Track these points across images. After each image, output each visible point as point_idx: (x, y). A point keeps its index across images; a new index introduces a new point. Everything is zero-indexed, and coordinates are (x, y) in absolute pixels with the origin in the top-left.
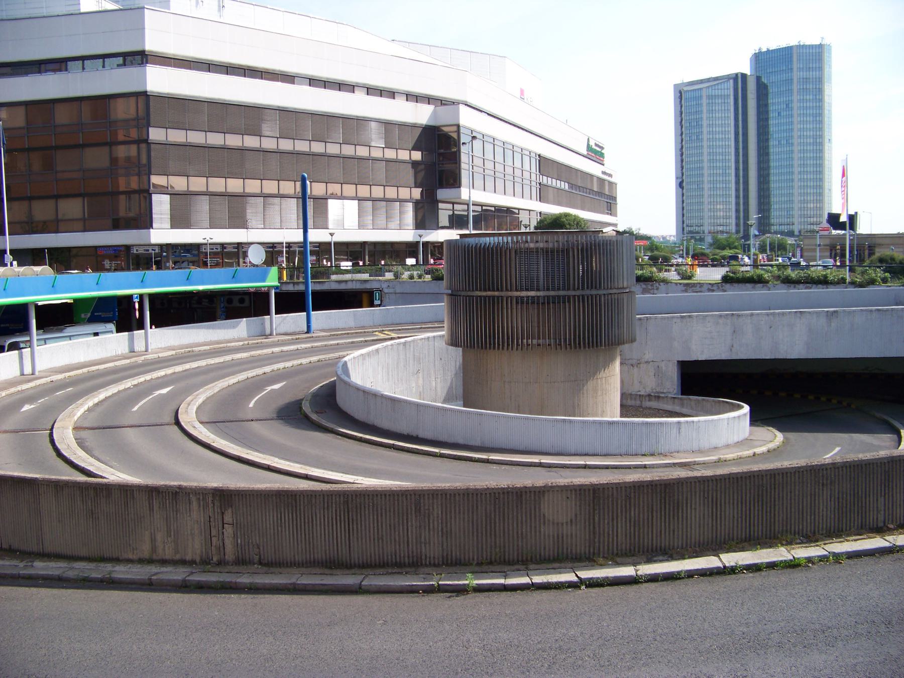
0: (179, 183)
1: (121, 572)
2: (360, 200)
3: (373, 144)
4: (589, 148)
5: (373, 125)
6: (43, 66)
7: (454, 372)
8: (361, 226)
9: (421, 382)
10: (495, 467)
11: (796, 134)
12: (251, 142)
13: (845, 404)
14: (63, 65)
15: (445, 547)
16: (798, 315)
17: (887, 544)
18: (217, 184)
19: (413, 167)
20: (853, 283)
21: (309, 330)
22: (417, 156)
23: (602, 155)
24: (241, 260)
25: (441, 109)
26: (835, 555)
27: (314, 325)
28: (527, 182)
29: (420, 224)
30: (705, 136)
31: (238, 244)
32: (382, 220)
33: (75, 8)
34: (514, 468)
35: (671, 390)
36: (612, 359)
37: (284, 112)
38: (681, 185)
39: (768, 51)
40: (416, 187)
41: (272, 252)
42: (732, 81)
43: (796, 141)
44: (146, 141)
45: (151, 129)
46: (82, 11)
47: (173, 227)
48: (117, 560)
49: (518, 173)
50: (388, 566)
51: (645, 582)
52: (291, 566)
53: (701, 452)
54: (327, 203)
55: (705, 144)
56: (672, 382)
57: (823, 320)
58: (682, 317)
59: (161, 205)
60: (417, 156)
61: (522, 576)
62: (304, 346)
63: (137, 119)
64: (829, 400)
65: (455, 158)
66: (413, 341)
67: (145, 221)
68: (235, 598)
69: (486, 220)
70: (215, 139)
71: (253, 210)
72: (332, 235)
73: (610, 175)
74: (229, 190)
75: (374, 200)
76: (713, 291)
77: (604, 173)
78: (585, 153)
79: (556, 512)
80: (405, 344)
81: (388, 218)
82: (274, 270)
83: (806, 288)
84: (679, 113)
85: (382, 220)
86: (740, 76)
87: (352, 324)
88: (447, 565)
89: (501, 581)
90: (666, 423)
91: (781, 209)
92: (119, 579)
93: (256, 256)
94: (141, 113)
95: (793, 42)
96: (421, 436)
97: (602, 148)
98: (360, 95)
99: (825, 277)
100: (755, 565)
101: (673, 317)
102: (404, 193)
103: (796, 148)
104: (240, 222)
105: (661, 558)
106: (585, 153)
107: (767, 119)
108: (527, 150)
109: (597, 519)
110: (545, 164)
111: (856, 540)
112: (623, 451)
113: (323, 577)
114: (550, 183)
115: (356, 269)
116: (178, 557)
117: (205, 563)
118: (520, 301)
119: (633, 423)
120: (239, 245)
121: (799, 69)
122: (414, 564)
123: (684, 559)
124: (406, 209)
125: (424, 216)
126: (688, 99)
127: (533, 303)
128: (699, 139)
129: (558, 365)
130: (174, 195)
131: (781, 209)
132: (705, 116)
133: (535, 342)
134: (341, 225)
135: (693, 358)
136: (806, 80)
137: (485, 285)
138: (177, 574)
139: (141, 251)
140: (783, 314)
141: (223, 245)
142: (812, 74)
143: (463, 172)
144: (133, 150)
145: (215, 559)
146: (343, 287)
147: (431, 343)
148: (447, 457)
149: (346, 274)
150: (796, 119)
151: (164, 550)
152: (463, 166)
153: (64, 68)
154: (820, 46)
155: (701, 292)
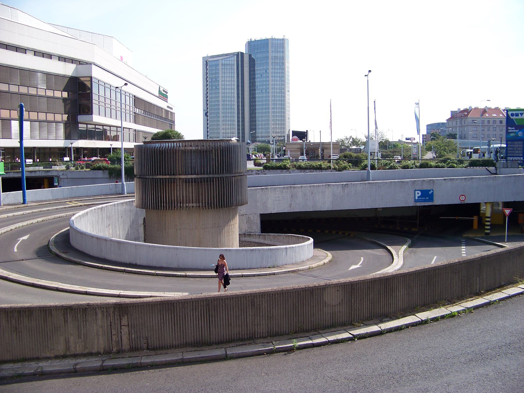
1: (47, 366)
3: (39, 87)
7: (129, 225)
9: (111, 231)
10: (192, 279)
11: (270, 87)
13: (347, 234)
15: (269, 326)
16: (327, 186)
17: (487, 301)
19: (63, 102)
20: (335, 169)
21: (24, 203)
22: (65, 95)
23: (167, 97)
26: (468, 308)
27: (27, 199)
28: (128, 112)
29: (68, 136)
30: (220, 87)
32: (45, 134)
34: (203, 279)
35: (257, 231)
38: (206, 114)
42: (235, 56)
43: (270, 91)
48: (38, 359)
50: (234, 341)
51: (386, 333)
52: (170, 348)
53: (297, 264)
54: (11, 123)
55: (220, 91)
56: (257, 227)
57: (340, 189)
60: (65, 95)
61: (320, 338)
62: (27, 212)
64: (337, 233)
65: (89, 97)
66: (106, 206)
68: (145, 373)
72: (111, 145)
73: (171, 108)
75: (40, 122)
76: (259, 174)
77: (168, 107)
78: (158, 95)
79: (332, 299)
80: (102, 208)
81: (49, 132)
83: (310, 172)
84: (205, 74)
85: (45, 134)
86: (240, 53)
87: (51, 198)
88: (270, 336)
89: (310, 342)
90: (280, 249)
91: (262, 129)
92: (50, 371)
95: (269, 37)
96: (138, 263)
97: (167, 93)
99: (321, 165)
100: (435, 318)
101: (257, 189)
102: (58, 117)
105: (386, 319)
106: (158, 95)
107: (254, 78)
109: (353, 301)
110: (137, 101)
111: (472, 300)
112: (258, 266)
113: (201, 352)
115: (35, 164)
116: (86, 351)
117: (108, 353)
118: (186, 181)
119: (264, 250)
122: (251, 338)
123: (399, 318)
124: (59, 127)
125: (70, 131)
126: (211, 66)
128: (217, 88)
129: (209, 218)
131: (262, 129)
132: (220, 75)
133: (191, 205)
136: (276, 57)
137: (171, 172)
138: (95, 363)
140: (319, 186)
142: (279, 55)
143: (94, 105)
145: (115, 350)
146: (33, 175)
147: (116, 208)
148: (179, 277)
149: (31, 167)
150: (270, 79)
151: (75, 347)
152: (94, 101)
154: (283, 40)
155: (252, 175)
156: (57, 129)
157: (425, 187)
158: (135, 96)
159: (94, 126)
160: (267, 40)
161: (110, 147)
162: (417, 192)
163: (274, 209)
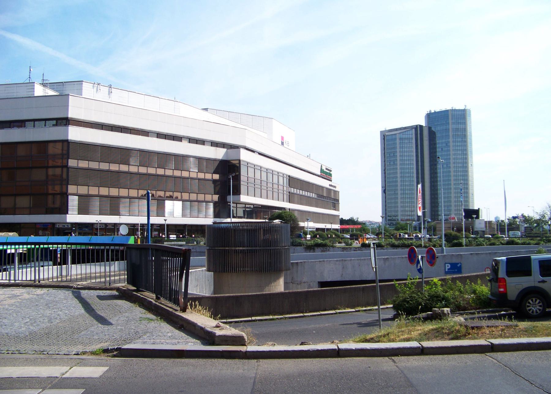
0: (83, 190)
2: (183, 201)
3: (191, 170)
4: (322, 170)
5: (192, 159)
6: (12, 124)
8: (184, 215)
12: (124, 168)
14: (23, 124)
18: (104, 191)
22: (216, 177)
23: (331, 175)
24: (116, 233)
25: (231, 151)
31: (115, 224)
32: (195, 213)
33: (32, 93)
36: (278, 278)
37: (142, 152)
38: (384, 191)
39: (435, 113)
40: (215, 194)
41: (133, 229)
42: (414, 130)
43: (452, 165)
44: (66, 166)
45: (69, 160)
46: (35, 95)
47: (79, 214)
49: (275, 186)
55: (398, 167)
58: (320, 261)
59: (73, 201)
60: (216, 177)
63: (62, 155)
65: (237, 179)
67: (64, 210)
69: (256, 213)
70: (104, 166)
71: (124, 206)
72: (165, 220)
73: (335, 187)
74: (111, 194)
77: (330, 185)
82: (132, 238)
85: (195, 213)
93: (124, 230)
94: (65, 152)
95: (449, 108)
97: (331, 171)
98: (185, 143)
102: (209, 197)
103: (452, 170)
104: (115, 212)
106: (319, 174)
108: (281, 173)
110: (292, 181)
114: (295, 192)
120: (115, 225)
121: (453, 123)
124: (209, 206)
125: (219, 211)
127: (241, 252)
128: (395, 164)
130: (80, 196)
132: (398, 150)
134: (172, 214)
135: (325, 280)
136: (457, 130)
139: (61, 226)
141: (106, 224)
142: (461, 126)
144: (58, 171)
152: (242, 183)
153: (23, 125)
154: (464, 110)
156: (207, 208)
157: (455, 261)
158: (289, 176)
159: (244, 205)
160: (447, 111)
161: (324, 227)
162: (447, 265)
163: (329, 278)
